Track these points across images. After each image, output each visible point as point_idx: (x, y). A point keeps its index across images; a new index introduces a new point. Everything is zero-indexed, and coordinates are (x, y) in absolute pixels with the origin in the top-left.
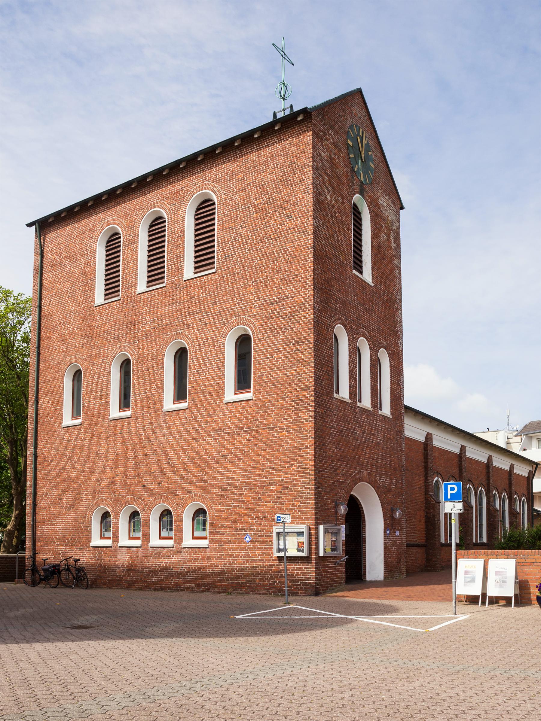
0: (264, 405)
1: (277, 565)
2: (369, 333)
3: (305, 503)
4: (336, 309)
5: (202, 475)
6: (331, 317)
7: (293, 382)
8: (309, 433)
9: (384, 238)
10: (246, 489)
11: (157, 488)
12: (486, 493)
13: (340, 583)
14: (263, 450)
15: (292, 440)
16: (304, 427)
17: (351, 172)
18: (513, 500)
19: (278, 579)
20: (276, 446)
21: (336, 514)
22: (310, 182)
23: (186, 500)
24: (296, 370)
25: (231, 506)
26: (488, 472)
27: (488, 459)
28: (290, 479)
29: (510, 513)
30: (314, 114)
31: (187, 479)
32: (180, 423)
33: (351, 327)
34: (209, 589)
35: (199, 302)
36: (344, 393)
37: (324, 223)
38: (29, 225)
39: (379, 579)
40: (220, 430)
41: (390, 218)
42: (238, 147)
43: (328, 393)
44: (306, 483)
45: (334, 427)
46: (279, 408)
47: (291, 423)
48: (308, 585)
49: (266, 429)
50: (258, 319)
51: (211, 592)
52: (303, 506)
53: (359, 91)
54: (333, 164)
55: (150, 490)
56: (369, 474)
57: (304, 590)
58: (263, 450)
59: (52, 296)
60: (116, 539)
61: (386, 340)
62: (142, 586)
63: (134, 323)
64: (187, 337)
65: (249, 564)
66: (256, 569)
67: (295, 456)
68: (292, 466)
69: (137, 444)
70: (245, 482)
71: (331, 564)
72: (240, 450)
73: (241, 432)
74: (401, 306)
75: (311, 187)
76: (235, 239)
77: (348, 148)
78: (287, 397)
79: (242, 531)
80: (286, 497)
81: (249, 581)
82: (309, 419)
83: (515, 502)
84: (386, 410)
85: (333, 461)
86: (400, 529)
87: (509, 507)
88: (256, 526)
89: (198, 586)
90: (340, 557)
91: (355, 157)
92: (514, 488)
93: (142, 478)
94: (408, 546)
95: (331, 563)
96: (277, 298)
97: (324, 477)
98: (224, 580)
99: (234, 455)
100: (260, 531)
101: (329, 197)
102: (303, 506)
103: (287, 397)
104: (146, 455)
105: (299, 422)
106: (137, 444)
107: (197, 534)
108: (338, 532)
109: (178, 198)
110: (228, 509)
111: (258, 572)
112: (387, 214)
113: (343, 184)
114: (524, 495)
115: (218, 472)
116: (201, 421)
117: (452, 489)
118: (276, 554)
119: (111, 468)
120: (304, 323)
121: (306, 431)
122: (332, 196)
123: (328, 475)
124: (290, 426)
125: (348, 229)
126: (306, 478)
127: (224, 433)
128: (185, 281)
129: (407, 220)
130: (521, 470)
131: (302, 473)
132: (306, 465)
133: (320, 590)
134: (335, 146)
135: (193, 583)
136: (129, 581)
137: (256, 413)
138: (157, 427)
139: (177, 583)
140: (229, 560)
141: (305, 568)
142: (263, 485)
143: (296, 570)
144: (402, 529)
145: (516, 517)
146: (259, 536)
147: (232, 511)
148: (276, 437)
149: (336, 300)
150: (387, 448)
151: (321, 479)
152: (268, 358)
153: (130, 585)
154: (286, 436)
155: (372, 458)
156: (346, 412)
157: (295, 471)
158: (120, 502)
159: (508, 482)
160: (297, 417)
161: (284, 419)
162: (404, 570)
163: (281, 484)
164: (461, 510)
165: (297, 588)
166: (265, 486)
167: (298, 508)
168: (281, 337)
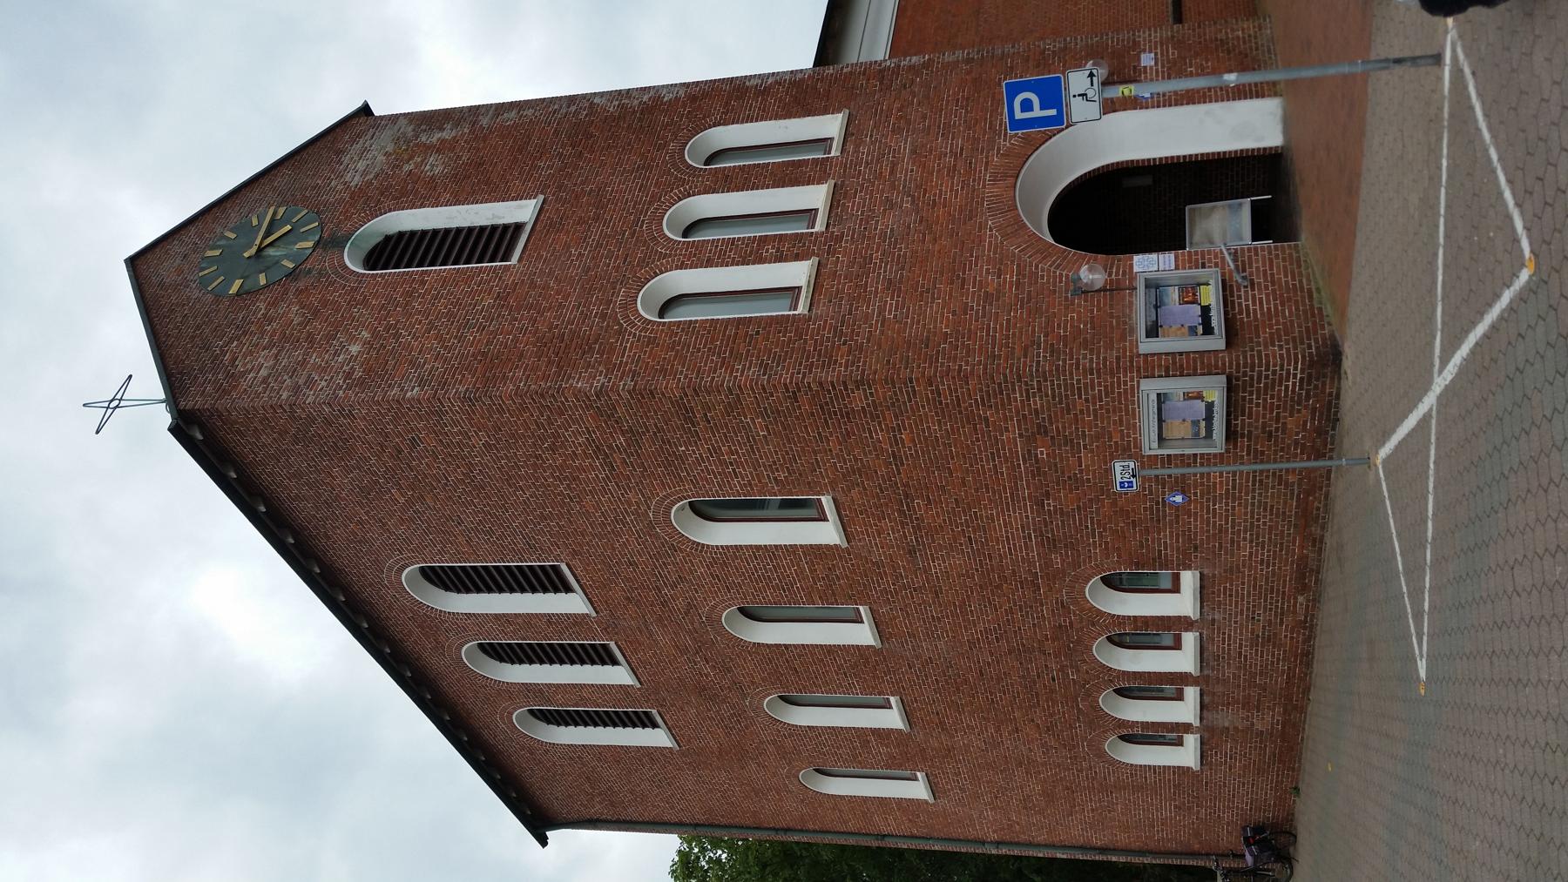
1: (1249, 440)
4: (603, 316)
6: (621, 332)
9: (435, 166)
13: (1299, 266)
14: (951, 474)
23: (1082, 610)
36: (797, 273)
37: (412, 363)
38: (543, 841)
39: (1279, 112)
41: (390, 148)
42: (296, 534)
45: (881, 311)
48: (1310, 375)
51: (1319, 567)
54: (284, 338)
55: (1062, 669)
58: (951, 474)
59: (672, 808)
61: (666, 144)
68: (986, 419)
76: (490, 532)
77: (248, 293)
84: (830, 126)
85: (965, 309)
86: (1136, 48)
90: (1223, 268)
91: (265, 270)
94: (1179, 18)
95: (1244, 300)
97: (1007, 337)
101: (355, 349)
108: (1154, 286)
112: (381, 158)
113: (324, 303)
117: (1027, 106)
122: (352, 339)
129: (396, 98)
134: (245, 333)
136: (1285, 711)
141: (1259, 382)
142: (1037, 472)
144: (1136, 44)
150: (924, 117)
153: (1295, 708)
162: (1249, 26)
163: (1030, 440)
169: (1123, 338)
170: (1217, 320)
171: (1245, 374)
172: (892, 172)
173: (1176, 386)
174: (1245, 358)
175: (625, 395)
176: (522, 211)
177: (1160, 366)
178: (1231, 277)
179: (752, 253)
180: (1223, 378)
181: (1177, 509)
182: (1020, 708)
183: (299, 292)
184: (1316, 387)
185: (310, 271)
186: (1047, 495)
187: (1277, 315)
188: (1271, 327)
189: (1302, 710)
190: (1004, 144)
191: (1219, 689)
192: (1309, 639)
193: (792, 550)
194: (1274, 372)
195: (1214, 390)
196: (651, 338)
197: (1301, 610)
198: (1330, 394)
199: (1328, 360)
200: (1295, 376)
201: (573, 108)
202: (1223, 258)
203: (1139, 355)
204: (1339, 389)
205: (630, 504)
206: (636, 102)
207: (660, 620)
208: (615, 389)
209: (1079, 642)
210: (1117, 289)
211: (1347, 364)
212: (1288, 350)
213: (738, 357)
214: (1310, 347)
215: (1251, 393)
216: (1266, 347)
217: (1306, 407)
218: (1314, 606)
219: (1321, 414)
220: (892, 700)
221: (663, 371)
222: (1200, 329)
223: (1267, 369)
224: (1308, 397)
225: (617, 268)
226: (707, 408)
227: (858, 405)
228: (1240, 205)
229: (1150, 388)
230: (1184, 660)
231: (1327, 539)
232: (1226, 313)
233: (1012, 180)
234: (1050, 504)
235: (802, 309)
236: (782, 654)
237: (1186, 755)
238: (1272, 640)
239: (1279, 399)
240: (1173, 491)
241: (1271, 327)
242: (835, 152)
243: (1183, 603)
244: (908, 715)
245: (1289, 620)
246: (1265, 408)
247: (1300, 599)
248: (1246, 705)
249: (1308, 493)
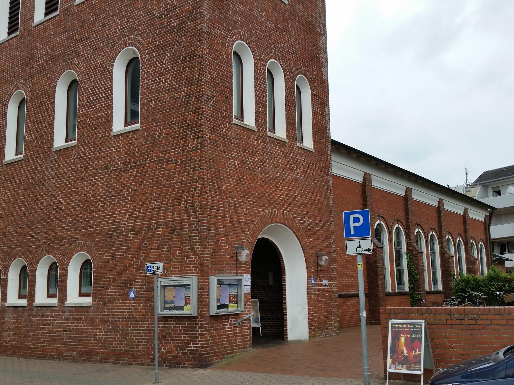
0: (151, 135)
3: (194, 248)
4: (236, 23)
5: (88, 221)
6: (229, 30)
7: (181, 106)
8: (197, 164)
10: (131, 234)
11: (45, 237)
12: (438, 238)
13: (242, 348)
14: (150, 187)
15: (180, 174)
16: (193, 156)
18: (469, 245)
19: (163, 346)
20: (163, 182)
21: (237, 261)
23: (72, 250)
24: (184, 91)
25: (117, 255)
26: (439, 216)
27: (439, 202)
28: (178, 220)
29: (467, 258)
31: (74, 225)
32: (68, 163)
34: (91, 358)
35: (89, 27)
36: (250, 120)
39: (303, 339)
40: (107, 167)
43: (224, 118)
44: (194, 224)
46: (167, 137)
47: (179, 153)
48: (195, 354)
49: (153, 162)
50: (146, 37)
51: (92, 361)
52: (191, 252)
55: (38, 240)
56: (284, 214)
57: (191, 361)
58: (150, 187)
62: (26, 353)
63: (29, 58)
64: (77, 66)
65: (133, 327)
66: (140, 333)
67: (184, 192)
69: (27, 189)
70: (131, 226)
71: (230, 325)
72: (127, 189)
73: (128, 167)
74: (325, 32)
78: (175, 124)
79: (127, 286)
80: (173, 241)
81: (132, 348)
82: (198, 146)
83: (472, 247)
84: (308, 143)
86: (330, 278)
87: (465, 252)
88: (141, 279)
89: (81, 354)
90: (244, 314)
92: (470, 233)
93: (30, 227)
94: (340, 296)
95: (230, 323)
96: (165, 11)
97: (219, 216)
98: (107, 347)
99: (120, 195)
100: (145, 285)
102: (191, 252)
103: (175, 124)
104: (35, 201)
105: (187, 152)
106: (27, 189)
107: (84, 290)
108: (238, 284)
110: (113, 259)
111: (142, 336)
114: (481, 240)
115: (104, 216)
116: (89, 158)
117: (356, 220)
118: (160, 312)
120: (193, 35)
121: (194, 162)
123: (224, 214)
124: (178, 157)
126: (195, 218)
127: (111, 171)
128: (76, 6)
130: (477, 215)
131: (190, 212)
132: (195, 202)
133: (213, 360)
135: (75, 351)
136: (14, 347)
137: (144, 145)
138: (46, 169)
139: (59, 350)
140: (112, 321)
141: (192, 331)
142: (150, 228)
143: (183, 334)
144: (331, 277)
145: (474, 263)
146: (144, 291)
147: (117, 261)
148: (163, 171)
151: (214, 218)
152: (156, 80)
154: (174, 169)
155: (288, 195)
156: (251, 141)
157: (183, 210)
159: (463, 227)
160: (185, 146)
161: (172, 149)
162: (336, 325)
164: (369, 250)
165: (184, 357)
166: (152, 229)
167: (185, 256)
168: (169, 55)
169: (217, 269)
170: (223, 311)
171: (197, 324)
172: (290, 169)
173: (193, 293)
174: (205, 324)
175: (200, 27)
177: (204, 285)
178: (239, 318)
179: (259, 100)
180: (196, 314)
181: (127, 295)
182: (16, 219)
184: (189, 357)
186: (138, 234)
187: (223, 338)
188: (218, 336)
189: (14, 354)
190: (298, 219)
191: (26, 315)
192: (53, 358)
194: (197, 338)
195: (189, 311)
196: (225, 45)
197: (69, 353)
198: (185, 364)
199: (202, 362)
200: (195, 347)
201: (321, 26)
202: (247, 314)
203: (209, 276)
204: (187, 368)
205: (139, 25)
206: (322, 55)
207: (71, 38)
208: (203, 22)
210: (237, 267)
211: (201, 371)
212: (208, 344)
213: (215, 86)
214: (209, 354)
215: (186, 327)
216: (210, 334)
217: (178, 353)
218: (70, 359)
219: (174, 360)
220: (22, 156)
221: (210, 48)
222: (219, 304)
223: (199, 334)
224: (183, 353)
225: (256, 34)
226: (191, 68)
227: (190, 143)
228: (258, 322)
229: (193, 281)
230: (41, 298)
231: (107, 365)
232: (225, 315)
233: (283, 222)
234: (132, 235)
235: (235, 121)
236: (49, 100)
237: (13, 299)
238: (53, 340)
239: (183, 340)
240: (136, 293)
241: (218, 336)
242: (298, 144)
243: (73, 298)
244: (12, 163)
245: (63, 348)
246: (179, 334)
247: (75, 353)
248: (17, 328)
249: (132, 355)
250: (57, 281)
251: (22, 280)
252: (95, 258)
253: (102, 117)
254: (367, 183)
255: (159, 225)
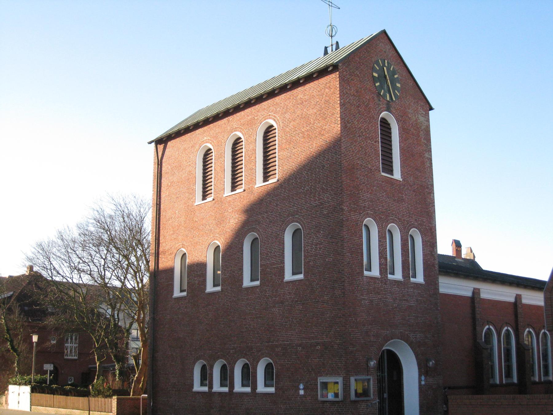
2: (398, 218)
6: (360, 213)
17: (377, 96)
22: (339, 116)
30: (340, 65)
33: (380, 218)
36: (375, 272)
38: (150, 143)
43: (358, 273)
45: (364, 299)
53: (384, 33)
56: (401, 332)
60: (211, 387)
75: (339, 119)
109: (251, 123)
119: (208, 331)
125: (375, 142)
129: (435, 119)
149: (364, 200)
158: (212, 360)
176: (397, 175)
183: (373, 98)
185: (379, 100)
193: (283, 262)
205: (301, 209)
209: (246, 354)
210: (367, 370)
229: (340, 380)
230: (238, 388)
234: (300, 349)
236: (239, 252)
237: (197, 387)
243: (261, 388)
250: (248, 376)
251: (223, 374)
252: (275, 362)
253: (277, 268)
254: (476, 296)
255: (318, 344)
